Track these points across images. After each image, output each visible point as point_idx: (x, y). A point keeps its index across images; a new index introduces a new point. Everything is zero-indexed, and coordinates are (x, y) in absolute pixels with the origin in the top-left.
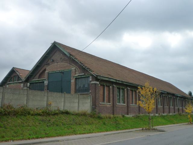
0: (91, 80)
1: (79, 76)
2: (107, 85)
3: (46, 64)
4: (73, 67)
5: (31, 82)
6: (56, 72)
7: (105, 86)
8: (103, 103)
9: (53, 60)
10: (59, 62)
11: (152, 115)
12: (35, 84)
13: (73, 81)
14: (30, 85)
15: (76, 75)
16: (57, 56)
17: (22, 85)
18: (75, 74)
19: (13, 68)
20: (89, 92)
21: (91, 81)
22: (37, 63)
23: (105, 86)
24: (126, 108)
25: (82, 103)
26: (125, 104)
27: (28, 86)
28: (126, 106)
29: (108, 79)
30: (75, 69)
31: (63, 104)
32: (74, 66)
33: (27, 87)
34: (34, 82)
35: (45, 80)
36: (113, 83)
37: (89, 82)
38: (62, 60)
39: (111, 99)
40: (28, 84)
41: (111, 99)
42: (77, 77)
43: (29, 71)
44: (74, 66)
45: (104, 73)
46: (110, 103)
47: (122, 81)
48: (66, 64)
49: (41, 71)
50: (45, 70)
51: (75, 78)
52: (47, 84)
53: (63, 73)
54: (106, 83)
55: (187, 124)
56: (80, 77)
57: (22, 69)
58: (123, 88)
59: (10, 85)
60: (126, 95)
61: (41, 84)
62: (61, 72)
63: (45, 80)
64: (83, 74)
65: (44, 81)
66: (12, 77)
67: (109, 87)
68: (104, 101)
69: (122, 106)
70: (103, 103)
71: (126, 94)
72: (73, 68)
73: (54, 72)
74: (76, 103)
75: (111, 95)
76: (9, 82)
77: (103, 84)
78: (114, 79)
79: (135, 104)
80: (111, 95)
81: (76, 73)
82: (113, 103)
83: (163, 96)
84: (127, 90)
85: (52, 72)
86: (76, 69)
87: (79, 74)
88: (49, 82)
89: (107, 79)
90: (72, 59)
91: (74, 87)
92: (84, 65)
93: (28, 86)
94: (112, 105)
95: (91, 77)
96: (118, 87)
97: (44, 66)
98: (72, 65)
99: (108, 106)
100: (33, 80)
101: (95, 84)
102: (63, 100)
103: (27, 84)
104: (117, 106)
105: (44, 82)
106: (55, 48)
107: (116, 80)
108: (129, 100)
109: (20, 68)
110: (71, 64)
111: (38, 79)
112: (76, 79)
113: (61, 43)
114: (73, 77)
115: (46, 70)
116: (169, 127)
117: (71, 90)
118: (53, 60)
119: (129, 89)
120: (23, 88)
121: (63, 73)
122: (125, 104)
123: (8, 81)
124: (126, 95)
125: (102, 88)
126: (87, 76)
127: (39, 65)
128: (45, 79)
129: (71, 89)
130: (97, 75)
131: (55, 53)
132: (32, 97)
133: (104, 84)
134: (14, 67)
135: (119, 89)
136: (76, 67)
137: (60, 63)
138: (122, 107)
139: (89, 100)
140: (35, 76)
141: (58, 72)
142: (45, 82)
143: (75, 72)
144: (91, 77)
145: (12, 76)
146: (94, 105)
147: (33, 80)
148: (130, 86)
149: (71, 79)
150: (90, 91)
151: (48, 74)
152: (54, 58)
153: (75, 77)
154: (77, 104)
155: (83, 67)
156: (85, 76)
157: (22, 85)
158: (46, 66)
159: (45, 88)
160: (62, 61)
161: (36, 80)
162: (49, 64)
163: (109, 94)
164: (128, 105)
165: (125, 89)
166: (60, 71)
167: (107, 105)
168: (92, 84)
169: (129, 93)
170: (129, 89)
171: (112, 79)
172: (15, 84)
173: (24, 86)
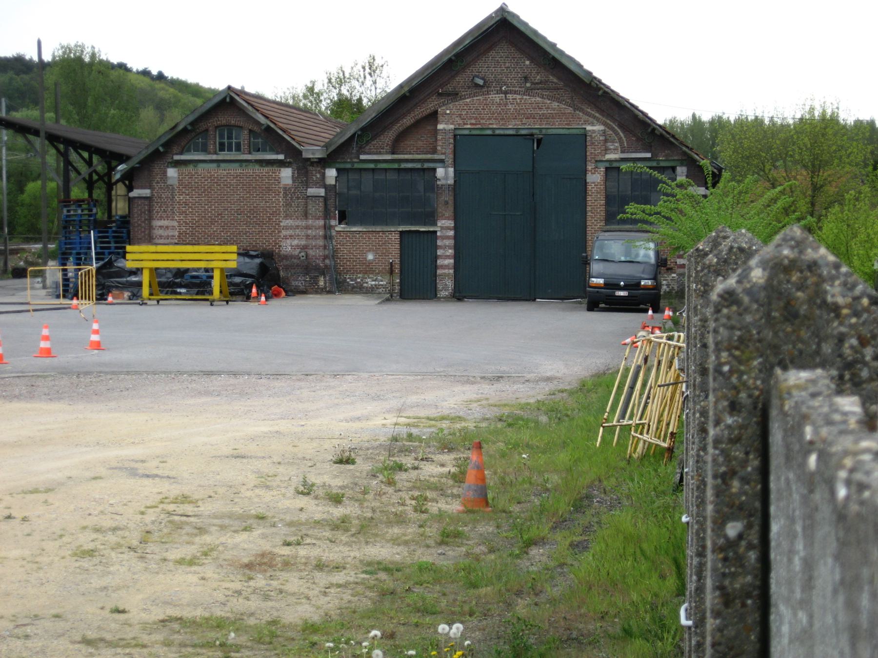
4: (591, 119)
6: (497, 132)
10: (515, 93)
18: (607, 150)
32: (594, 117)
35: (442, 161)
38: (528, 85)
44: (594, 117)
48: (555, 104)
52: (451, 181)
53: (539, 142)
63: (442, 161)
64: (649, 155)
65: (431, 165)
87: (622, 152)
90: (650, 130)
98: (587, 114)
100: (362, 157)
103: (323, 176)
105: (434, 170)
106: (502, 33)
110: (582, 110)
116: (22, 304)
117: (589, 214)
126: (662, 164)
128: (443, 157)
129: (589, 208)
136: (605, 124)
137: (518, 97)
142: (440, 172)
151: (455, 136)
153: (608, 165)
160: (528, 89)
172: (237, 165)
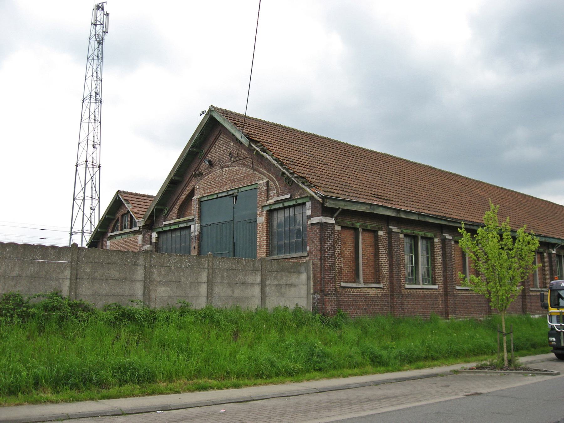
0: (309, 212)
1: (277, 202)
2: (369, 228)
3: (195, 176)
5: (160, 230)
6: (219, 195)
7: (360, 230)
8: (354, 285)
9: (210, 162)
10: (227, 166)
11: (537, 316)
12: (169, 235)
13: (261, 220)
14: (158, 238)
15: (271, 201)
16: (219, 150)
17: (140, 237)
18: (268, 197)
19: (119, 192)
20: (306, 250)
21: (309, 217)
22: (170, 173)
23: (360, 230)
24: (440, 299)
25: (277, 285)
26: (436, 287)
27: (154, 240)
28: (441, 290)
29: (369, 207)
30: (268, 182)
31: (203, 289)
32: (264, 174)
33: (151, 243)
34: (168, 228)
35: (192, 220)
36: (387, 220)
37: (305, 218)
39: (385, 271)
40: (154, 235)
41: (385, 271)
42: (273, 207)
43: (152, 197)
44: (264, 174)
45: (358, 195)
46: (379, 283)
47: (419, 214)
49: (183, 197)
50: (192, 193)
51: (268, 211)
52: (197, 233)
54: (356, 219)
55: (493, 367)
56: (281, 205)
57: (144, 196)
58: (429, 235)
59: (113, 240)
60: (439, 258)
61: (183, 233)
62: (233, 194)
63: (192, 220)
65: (189, 224)
66: (118, 220)
67: (375, 232)
68: (356, 278)
69: (427, 292)
70: (354, 285)
71: (440, 253)
72: (262, 179)
73: (215, 196)
74: (252, 284)
75: (384, 259)
76: (113, 231)
77: (353, 224)
78: (388, 208)
79: (541, 287)
80: (384, 259)
81: (271, 193)
82: (391, 283)
83: (550, 255)
84: (444, 240)
85: (210, 198)
86: (271, 183)
88: (202, 227)
89: (363, 209)
91: (258, 236)
92: (287, 169)
93: (154, 240)
94: (387, 291)
95: (309, 204)
96: (409, 232)
97: (189, 182)
98: (260, 172)
99: (372, 292)
100: (164, 223)
101: (321, 224)
102: (204, 277)
103: (151, 236)
104: (405, 292)
105: (190, 227)
106: (212, 127)
107: (398, 211)
108: (449, 273)
109: (138, 192)
110: (257, 170)
111: (177, 218)
112: (270, 212)
113: (233, 111)
114: (263, 207)
115: (196, 192)
118: (210, 162)
119: (451, 238)
120: (143, 246)
121: (236, 197)
122: (436, 287)
123: (110, 230)
124: (439, 258)
125: (348, 236)
126: (299, 202)
127: (176, 178)
128: (193, 217)
129: (258, 244)
130: (323, 198)
131: (216, 140)
132: (88, 270)
133: (357, 225)
134: (121, 190)
135: (414, 238)
137: (228, 169)
138: (425, 296)
139: (304, 276)
140: (170, 211)
141: (225, 194)
142: (193, 227)
143: (268, 190)
144: (310, 203)
145: (119, 215)
146: (321, 287)
147: (164, 223)
148: (398, 221)
149: (256, 215)
150: (308, 248)
152: (213, 155)
153: (268, 208)
154: (257, 290)
155: (284, 173)
156: (294, 203)
157: (140, 237)
158: (194, 180)
159: (194, 245)
161: (173, 221)
162: (202, 174)
163: (376, 254)
164: (445, 288)
165: (436, 240)
166: (230, 193)
167: (368, 290)
168: (312, 224)
169: (448, 250)
170: (451, 238)
171: (381, 209)
173: (144, 240)
